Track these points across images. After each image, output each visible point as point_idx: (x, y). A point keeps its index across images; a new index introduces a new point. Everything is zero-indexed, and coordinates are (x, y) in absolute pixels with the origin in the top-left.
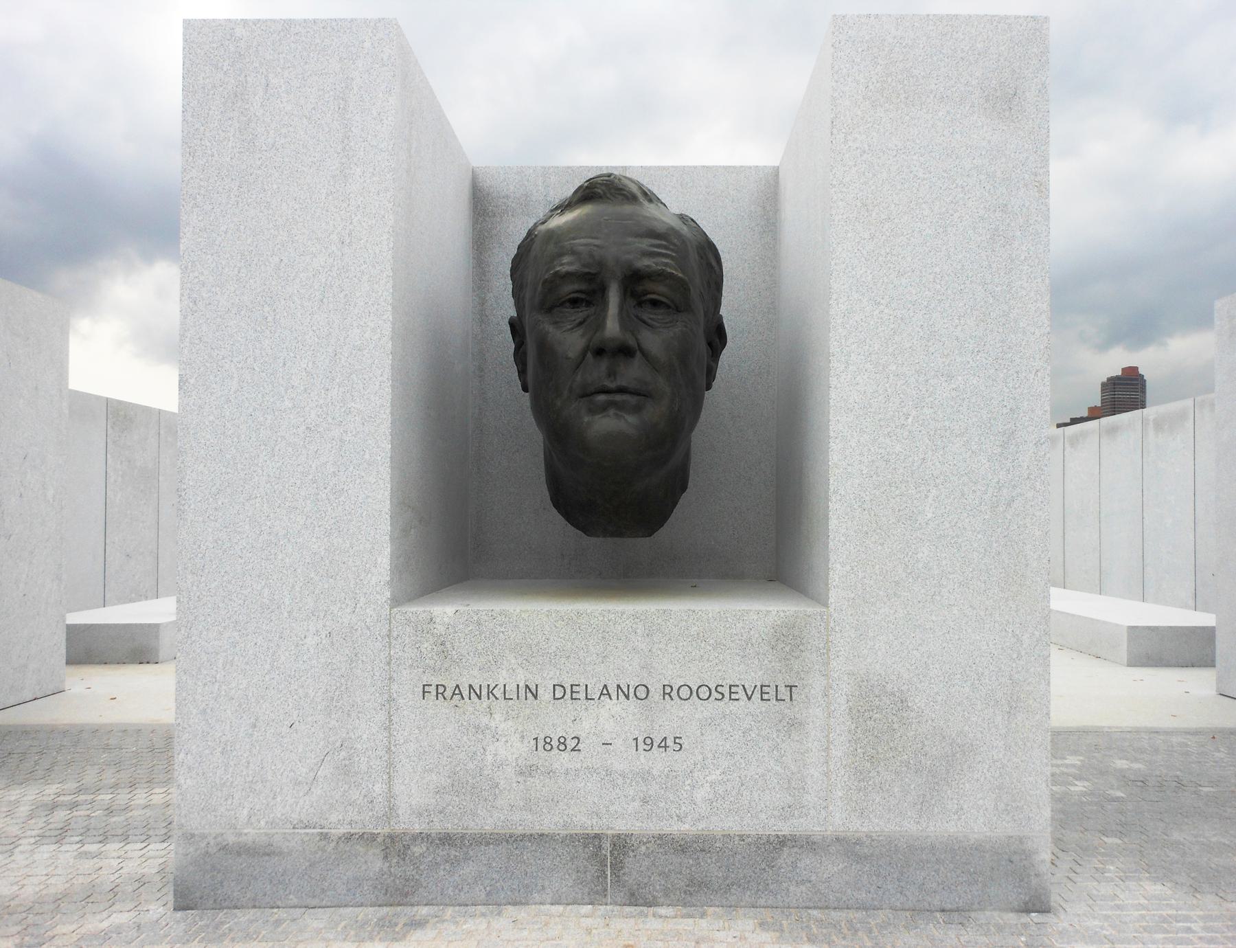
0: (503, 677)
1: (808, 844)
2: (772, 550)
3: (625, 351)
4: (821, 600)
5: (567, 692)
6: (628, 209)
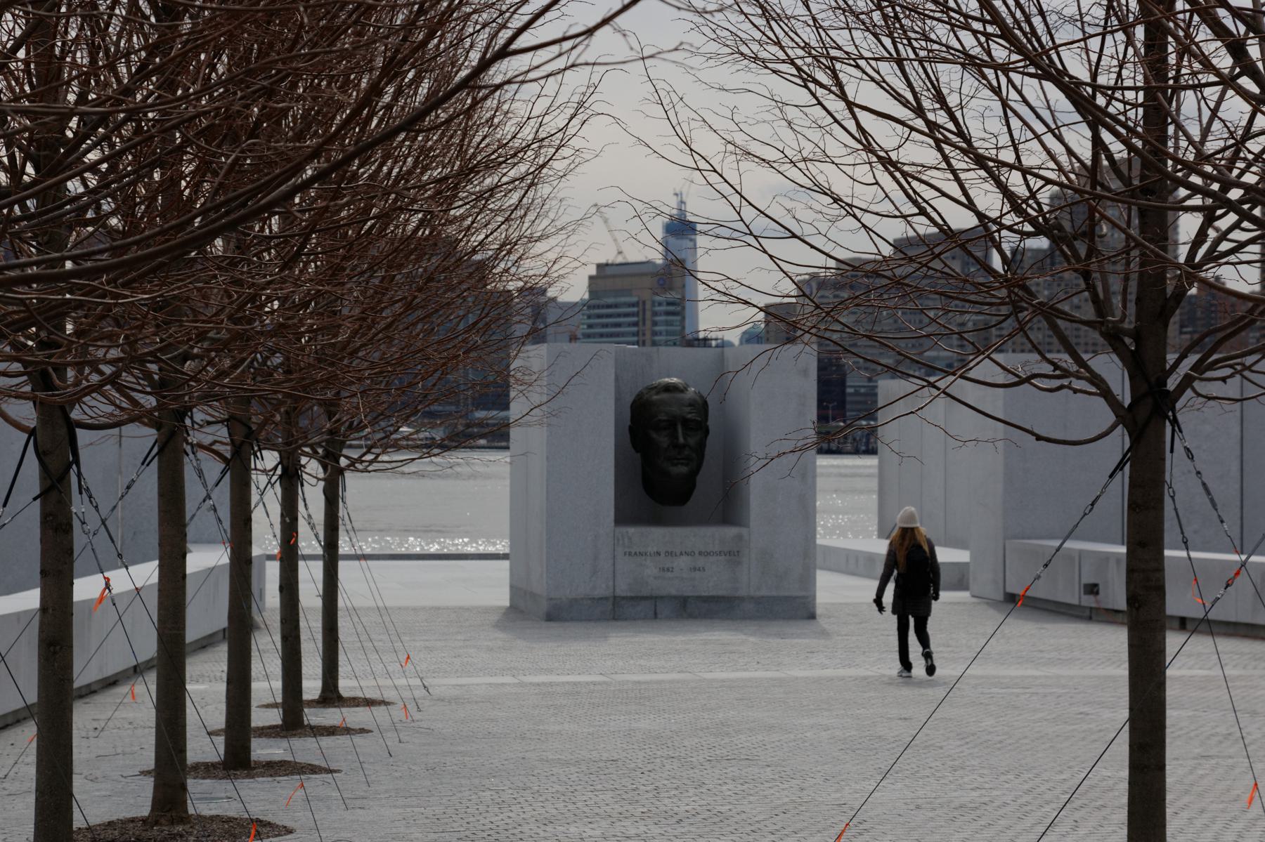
0: (649, 549)
1: (742, 599)
2: (728, 509)
3: (684, 446)
4: (747, 525)
5: (670, 554)
6: (681, 395)
